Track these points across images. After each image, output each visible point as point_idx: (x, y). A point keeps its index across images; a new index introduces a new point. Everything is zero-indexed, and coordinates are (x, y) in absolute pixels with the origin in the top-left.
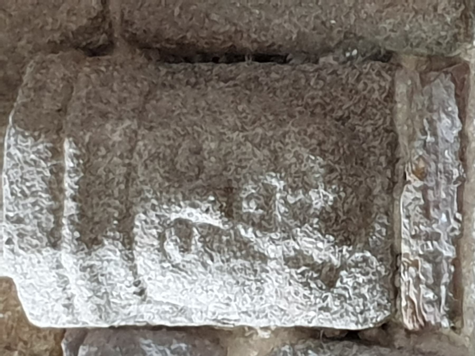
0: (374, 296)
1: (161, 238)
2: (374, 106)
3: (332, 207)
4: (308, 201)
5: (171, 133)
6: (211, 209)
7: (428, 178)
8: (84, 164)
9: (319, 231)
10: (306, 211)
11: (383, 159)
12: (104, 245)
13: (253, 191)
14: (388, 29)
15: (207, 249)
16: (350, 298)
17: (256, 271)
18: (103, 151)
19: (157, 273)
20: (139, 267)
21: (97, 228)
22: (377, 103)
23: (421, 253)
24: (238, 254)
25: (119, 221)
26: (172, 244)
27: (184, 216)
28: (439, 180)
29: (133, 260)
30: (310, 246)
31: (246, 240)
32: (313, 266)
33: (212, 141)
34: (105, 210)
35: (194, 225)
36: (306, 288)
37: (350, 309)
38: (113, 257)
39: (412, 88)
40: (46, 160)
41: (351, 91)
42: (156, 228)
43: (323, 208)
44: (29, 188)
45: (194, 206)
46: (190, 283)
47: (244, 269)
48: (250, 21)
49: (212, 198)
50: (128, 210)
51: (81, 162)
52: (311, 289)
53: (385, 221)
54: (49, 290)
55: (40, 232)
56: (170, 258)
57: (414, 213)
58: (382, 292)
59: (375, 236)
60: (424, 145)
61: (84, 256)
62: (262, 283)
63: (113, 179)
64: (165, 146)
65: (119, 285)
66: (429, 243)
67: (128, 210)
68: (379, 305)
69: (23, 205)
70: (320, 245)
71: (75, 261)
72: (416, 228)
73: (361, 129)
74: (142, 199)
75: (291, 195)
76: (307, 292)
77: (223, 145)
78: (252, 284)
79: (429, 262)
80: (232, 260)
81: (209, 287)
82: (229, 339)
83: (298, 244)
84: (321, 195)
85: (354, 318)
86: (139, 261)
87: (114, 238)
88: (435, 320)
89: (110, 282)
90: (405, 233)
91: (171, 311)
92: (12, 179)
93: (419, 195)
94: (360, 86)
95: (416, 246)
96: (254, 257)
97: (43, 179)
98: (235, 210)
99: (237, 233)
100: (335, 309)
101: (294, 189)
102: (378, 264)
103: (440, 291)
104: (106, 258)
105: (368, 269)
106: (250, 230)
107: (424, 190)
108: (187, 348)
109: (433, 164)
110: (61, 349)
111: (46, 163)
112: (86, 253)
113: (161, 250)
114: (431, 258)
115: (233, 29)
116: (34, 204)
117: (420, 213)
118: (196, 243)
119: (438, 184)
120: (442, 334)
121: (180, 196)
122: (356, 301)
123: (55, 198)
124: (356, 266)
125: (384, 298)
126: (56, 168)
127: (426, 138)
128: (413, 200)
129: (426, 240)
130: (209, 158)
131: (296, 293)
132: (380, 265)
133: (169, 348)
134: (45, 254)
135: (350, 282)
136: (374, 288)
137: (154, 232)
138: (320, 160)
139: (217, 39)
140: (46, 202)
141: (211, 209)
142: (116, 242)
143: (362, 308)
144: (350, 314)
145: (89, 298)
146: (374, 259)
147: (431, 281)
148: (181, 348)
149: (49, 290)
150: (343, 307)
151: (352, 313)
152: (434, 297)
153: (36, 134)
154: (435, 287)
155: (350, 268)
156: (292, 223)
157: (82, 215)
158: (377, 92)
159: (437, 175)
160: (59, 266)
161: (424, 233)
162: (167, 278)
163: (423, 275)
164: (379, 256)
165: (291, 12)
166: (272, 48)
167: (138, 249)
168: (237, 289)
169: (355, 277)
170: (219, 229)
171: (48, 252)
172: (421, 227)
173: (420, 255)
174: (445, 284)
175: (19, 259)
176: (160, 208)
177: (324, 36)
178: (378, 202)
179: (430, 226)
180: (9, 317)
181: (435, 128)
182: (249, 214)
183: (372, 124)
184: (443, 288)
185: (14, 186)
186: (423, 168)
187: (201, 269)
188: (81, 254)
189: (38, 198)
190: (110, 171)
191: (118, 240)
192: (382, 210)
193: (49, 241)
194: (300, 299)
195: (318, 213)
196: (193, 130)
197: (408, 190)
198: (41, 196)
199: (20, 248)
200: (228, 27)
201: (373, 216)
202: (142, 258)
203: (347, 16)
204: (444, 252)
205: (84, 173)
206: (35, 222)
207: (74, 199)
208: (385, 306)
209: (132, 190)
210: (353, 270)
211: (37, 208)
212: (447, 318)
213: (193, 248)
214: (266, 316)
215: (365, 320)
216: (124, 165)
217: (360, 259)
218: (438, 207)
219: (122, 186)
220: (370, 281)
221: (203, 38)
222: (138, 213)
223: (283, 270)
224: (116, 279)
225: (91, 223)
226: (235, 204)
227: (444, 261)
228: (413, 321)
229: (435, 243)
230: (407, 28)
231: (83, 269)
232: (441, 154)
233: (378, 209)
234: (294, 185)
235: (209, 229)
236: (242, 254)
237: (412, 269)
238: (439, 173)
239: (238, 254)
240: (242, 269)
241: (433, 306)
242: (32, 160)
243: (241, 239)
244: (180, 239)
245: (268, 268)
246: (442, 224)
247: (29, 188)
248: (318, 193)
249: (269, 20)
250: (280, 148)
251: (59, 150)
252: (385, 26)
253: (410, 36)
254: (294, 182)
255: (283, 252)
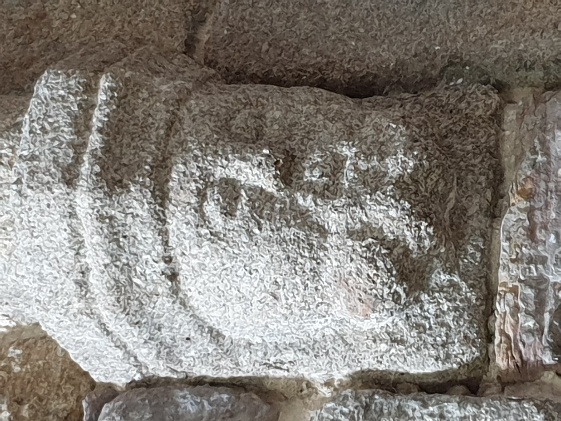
0: (460, 326)
1: (201, 195)
2: (476, 124)
3: (411, 176)
4: (383, 169)
5: (231, 99)
6: (264, 163)
7: (536, 198)
8: (119, 98)
9: (393, 197)
10: (380, 180)
11: (483, 178)
12: (129, 191)
13: (319, 160)
14: (498, 50)
15: (255, 215)
16: (431, 328)
17: (311, 245)
18: (145, 94)
19: (192, 243)
20: (171, 234)
21: (124, 169)
22: (480, 121)
23: (522, 278)
24: (292, 223)
25: (152, 167)
26: (212, 204)
27: (232, 174)
28: (549, 200)
29: (164, 222)
30: (381, 216)
31: (305, 209)
32: (382, 241)
33: (277, 109)
34: (136, 153)
35: (242, 186)
36: (371, 265)
37: (430, 340)
38: (140, 212)
39: (524, 109)
40: (76, 95)
41: (451, 112)
42: (196, 181)
43: (401, 176)
44: (51, 124)
45: (244, 159)
46: (230, 258)
47: (297, 240)
48: (344, 52)
49: (266, 151)
50: (164, 160)
51: (116, 95)
52: (377, 268)
53: (481, 245)
54: (59, 255)
55: (54, 168)
56: (210, 223)
57: (516, 236)
58: (471, 322)
59: (466, 259)
60: (534, 165)
61: (102, 195)
62: (318, 263)
63: (153, 123)
64: (221, 107)
65: (145, 257)
66: (532, 267)
67: (164, 160)
68: (466, 337)
69: (40, 141)
70: (393, 213)
71: (91, 201)
72: (518, 250)
73: (459, 147)
74: (183, 150)
75: (363, 161)
76: (373, 272)
77: (290, 116)
78: (306, 262)
79: (531, 287)
80: (283, 229)
81: (253, 266)
82: (283, 404)
83: (366, 215)
84: (399, 161)
85: (433, 352)
86: (172, 225)
87: (143, 185)
88: (535, 355)
89: (134, 250)
90: (504, 257)
91: (215, 353)
92: (34, 118)
93: (524, 216)
94: (463, 105)
95: (516, 270)
96: (311, 228)
97: (69, 114)
98: (295, 180)
99: (293, 201)
100: (412, 341)
101: (368, 157)
102: (468, 290)
103: (543, 319)
104: (131, 210)
105: (455, 295)
106: (310, 196)
107: (530, 211)
108: (229, 399)
109: (543, 185)
110: (81, 407)
111: (75, 97)
112: (105, 193)
113: (199, 210)
114: (534, 285)
115: (325, 60)
116: (53, 140)
117: (524, 235)
118: (242, 208)
119: (547, 205)
120: (544, 383)
121: (229, 149)
122: (437, 330)
123: (78, 133)
124: (441, 290)
125: (473, 331)
126: (86, 104)
127: (536, 158)
128: (516, 221)
129: (528, 263)
130: (272, 125)
131: (359, 273)
132: (471, 292)
133: (208, 400)
134: (57, 191)
135: (432, 309)
136: (461, 316)
137: (193, 186)
138: (403, 129)
139: (305, 72)
140: (67, 136)
141: (264, 163)
142: (144, 190)
143: (444, 338)
144: (429, 346)
145: (106, 266)
146: (464, 285)
147: (532, 308)
148: (222, 399)
149: (59, 255)
150: (421, 339)
151: (432, 345)
152: (534, 324)
153: (70, 71)
154: (537, 314)
155: (433, 293)
156: (359, 188)
157: (107, 149)
158: (481, 110)
159: (547, 195)
160: (72, 215)
161: (528, 256)
162: (203, 250)
163: (523, 301)
164: (470, 282)
165: (391, 41)
166: (366, 81)
167: (171, 208)
168: (286, 267)
169: (439, 303)
170: (272, 196)
171: (59, 189)
172: (524, 249)
173: (520, 281)
174: (550, 312)
175: (27, 204)
176: (203, 160)
177: (427, 63)
178: (473, 223)
179: (535, 248)
180: (27, 372)
181: (548, 149)
182: (311, 182)
183: (473, 143)
184: (547, 317)
185: (35, 124)
186: (531, 189)
187: (245, 238)
188: (99, 192)
189: (60, 133)
190: (150, 115)
191: (147, 187)
192: (478, 232)
193: (64, 177)
194: (363, 282)
195: (394, 181)
196: (257, 101)
197: (511, 212)
198: (62, 131)
199: (29, 187)
200: (319, 59)
201: (466, 238)
202: (175, 220)
203: (454, 40)
204: (550, 277)
205: (118, 107)
206: (51, 157)
207: (100, 131)
208: (474, 341)
209: (173, 141)
210: (437, 295)
211: (56, 143)
212: (551, 350)
213: (238, 213)
214: (327, 353)
215: (448, 356)
216: (168, 112)
217: (445, 283)
218: (546, 228)
219: (162, 132)
220: (456, 309)
221: (291, 71)
222: (176, 163)
223: (345, 243)
224: (141, 247)
225: (117, 163)
226: (295, 174)
227: (550, 288)
228: (508, 358)
229: (540, 266)
230: (522, 46)
231: (101, 218)
232: (553, 173)
233: (473, 231)
234: (368, 152)
235: (261, 194)
236: (296, 223)
237: (509, 296)
238: (549, 193)
239: (292, 223)
240: (294, 240)
241: (533, 335)
242: (60, 96)
243: (298, 209)
244: (224, 199)
245: (327, 245)
246: (549, 246)
247: (51, 124)
248: (397, 159)
249: (365, 50)
250: (358, 126)
251: (93, 86)
252: (496, 46)
253: (524, 55)
254: (369, 149)
255: (347, 223)
